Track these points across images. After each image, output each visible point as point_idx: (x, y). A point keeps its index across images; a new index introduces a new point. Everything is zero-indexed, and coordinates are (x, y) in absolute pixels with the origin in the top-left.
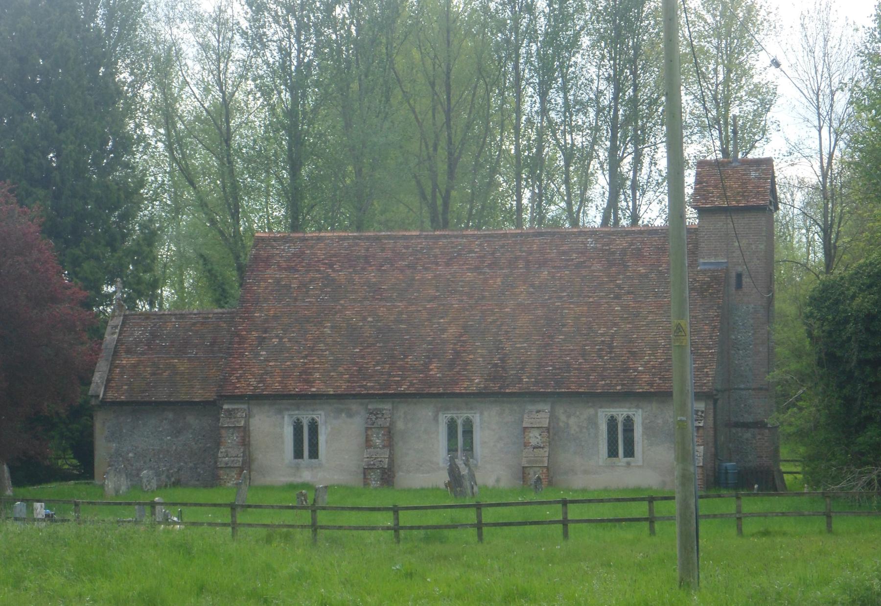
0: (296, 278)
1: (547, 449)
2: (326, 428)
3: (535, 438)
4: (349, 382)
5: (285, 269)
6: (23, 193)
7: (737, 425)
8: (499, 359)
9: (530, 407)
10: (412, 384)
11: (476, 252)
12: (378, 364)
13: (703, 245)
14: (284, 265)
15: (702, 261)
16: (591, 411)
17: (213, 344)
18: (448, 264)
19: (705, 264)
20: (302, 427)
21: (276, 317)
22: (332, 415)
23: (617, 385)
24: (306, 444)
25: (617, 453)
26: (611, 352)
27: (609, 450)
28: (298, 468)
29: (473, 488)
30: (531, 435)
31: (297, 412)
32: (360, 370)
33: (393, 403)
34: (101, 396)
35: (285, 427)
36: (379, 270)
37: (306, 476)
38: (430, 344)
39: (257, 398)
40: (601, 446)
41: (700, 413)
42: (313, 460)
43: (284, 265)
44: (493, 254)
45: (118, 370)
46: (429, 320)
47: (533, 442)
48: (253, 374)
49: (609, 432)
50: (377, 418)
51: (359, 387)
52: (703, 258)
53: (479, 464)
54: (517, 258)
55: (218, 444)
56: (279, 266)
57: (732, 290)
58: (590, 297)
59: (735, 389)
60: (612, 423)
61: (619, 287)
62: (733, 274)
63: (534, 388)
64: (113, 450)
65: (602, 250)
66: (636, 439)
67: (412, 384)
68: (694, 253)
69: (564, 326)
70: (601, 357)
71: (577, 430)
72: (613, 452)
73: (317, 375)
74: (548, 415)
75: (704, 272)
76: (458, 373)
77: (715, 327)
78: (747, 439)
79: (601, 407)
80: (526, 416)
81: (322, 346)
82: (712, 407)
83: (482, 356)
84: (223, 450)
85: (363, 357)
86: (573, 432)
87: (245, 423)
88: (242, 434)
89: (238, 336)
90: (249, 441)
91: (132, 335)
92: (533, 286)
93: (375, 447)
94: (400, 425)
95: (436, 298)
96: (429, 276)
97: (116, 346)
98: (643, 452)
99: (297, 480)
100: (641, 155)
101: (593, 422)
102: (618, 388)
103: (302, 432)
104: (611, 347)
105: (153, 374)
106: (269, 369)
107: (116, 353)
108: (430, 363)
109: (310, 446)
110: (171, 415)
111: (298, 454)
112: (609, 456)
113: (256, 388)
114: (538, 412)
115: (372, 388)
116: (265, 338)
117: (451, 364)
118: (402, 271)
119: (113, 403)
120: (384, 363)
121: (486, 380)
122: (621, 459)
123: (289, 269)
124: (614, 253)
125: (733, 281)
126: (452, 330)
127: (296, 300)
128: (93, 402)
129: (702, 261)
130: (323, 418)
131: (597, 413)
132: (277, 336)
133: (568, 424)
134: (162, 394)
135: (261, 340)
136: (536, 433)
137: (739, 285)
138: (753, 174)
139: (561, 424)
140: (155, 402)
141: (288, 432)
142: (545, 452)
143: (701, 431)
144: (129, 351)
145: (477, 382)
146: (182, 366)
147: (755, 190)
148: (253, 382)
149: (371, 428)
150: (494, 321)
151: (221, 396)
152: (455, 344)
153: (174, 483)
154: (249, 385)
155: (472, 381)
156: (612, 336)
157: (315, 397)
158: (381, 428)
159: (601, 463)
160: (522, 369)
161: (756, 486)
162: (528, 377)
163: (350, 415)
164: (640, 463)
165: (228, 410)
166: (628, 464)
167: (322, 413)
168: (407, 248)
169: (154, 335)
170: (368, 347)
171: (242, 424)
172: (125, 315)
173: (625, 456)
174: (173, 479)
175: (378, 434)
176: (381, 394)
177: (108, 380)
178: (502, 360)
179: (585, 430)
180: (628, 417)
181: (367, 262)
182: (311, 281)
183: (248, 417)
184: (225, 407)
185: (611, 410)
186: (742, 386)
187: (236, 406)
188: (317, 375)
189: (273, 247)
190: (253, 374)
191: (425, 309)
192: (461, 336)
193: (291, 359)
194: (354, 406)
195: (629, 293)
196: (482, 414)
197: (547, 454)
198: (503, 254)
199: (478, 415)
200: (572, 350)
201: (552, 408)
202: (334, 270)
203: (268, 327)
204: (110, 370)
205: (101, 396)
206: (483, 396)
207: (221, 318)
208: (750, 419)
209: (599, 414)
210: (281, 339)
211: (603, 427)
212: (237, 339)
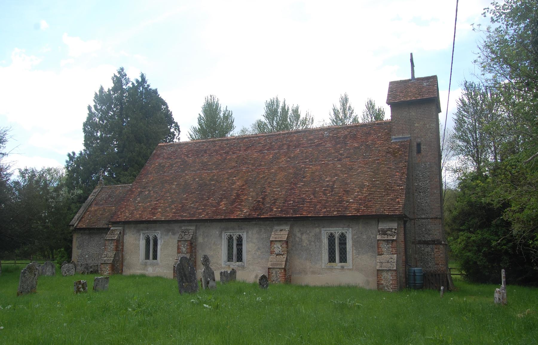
1: (285, 256)
2: (161, 242)
3: (278, 248)
7: (420, 242)
8: (262, 198)
9: (276, 228)
10: (207, 214)
13: (394, 127)
14: (166, 157)
15: (394, 137)
16: (317, 230)
18: (245, 150)
19: (396, 139)
23: (334, 211)
24: (152, 251)
25: (335, 260)
26: (332, 191)
27: (330, 258)
28: (146, 265)
29: (208, 283)
30: (275, 246)
33: (196, 226)
34: (75, 225)
35: (141, 240)
36: (210, 155)
37: (150, 271)
38: (224, 191)
39: (126, 223)
41: (393, 230)
42: (154, 261)
43: (166, 157)
46: (228, 178)
47: (277, 251)
49: (329, 245)
52: (395, 135)
57: (415, 153)
58: (322, 161)
59: (418, 218)
60: (331, 238)
61: (341, 154)
62: (415, 144)
63: (279, 215)
65: (333, 137)
66: (348, 249)
68: (389, 134)
69: (304, 177)
70: (325, 194)
71: (308, 243)
72: (332, 259)
74: (287, 233)
75: (395, 143)
76: (235, 207)
77: (404, 173)
78: (428, 252)
80: (273, 233)
81: (168, 194)
82: (403, 226)
83: (252, 197)
85: (187, 200)
86: (305, 244)
93: (183, 253)
94: (200, 240)
98: (353, 260)
100: (425, 241)
101: (318, 238)
102: (335, 213)
104: (332, 188)
105: (102, 214)
108: (221, 201)
111: (147, 257)
112: (330, 262)
114: (281, 230)
115: (185, 216)
117: (234, 202)
118: (221, 155)
119: (80, 229)
121: (251, 210)
122: (338, 264)
124: (339, 138)
125: (415, 148)
129: (394, 137)
131: (321, 231)
133: (301, 239)
136: (278, 245)
137: (419, 151)
138: (425, 84)
139: (297, 239)
140: (96, 228)
141: (142, 243)
142: (283, 258)
143: (394, 243)
145: (246, 211)
147: (427, 91)
149: (181, 241)
150: (264, 177)
152: (238, 190)
153: (91, 272)
155: (242, 211)
156: (334, 182)
157: (155, 222)
158: (186, 241)
160: (274, 203)
161: (442, 288)
164: (351, 267)
166: (343, 267)
168: (227, 144)
175: (184, 245)
178: (264, 199)
179: (313, 243)
180: (342, 234)
181: (205, 152)
185: (331, 229)
186: (423, 216)
189: (164, 149)
191: (227, 173)
192: (243, 186)
195: (347, 157)
197: (285, 259)
198: (276, 143)
199: (245, 233)
200: (307, 191)
201: (291, 228)
205: (75, 225)
206: (247, 220)
208: (429, 238)
209: (322, 232)
211: (325, 241)
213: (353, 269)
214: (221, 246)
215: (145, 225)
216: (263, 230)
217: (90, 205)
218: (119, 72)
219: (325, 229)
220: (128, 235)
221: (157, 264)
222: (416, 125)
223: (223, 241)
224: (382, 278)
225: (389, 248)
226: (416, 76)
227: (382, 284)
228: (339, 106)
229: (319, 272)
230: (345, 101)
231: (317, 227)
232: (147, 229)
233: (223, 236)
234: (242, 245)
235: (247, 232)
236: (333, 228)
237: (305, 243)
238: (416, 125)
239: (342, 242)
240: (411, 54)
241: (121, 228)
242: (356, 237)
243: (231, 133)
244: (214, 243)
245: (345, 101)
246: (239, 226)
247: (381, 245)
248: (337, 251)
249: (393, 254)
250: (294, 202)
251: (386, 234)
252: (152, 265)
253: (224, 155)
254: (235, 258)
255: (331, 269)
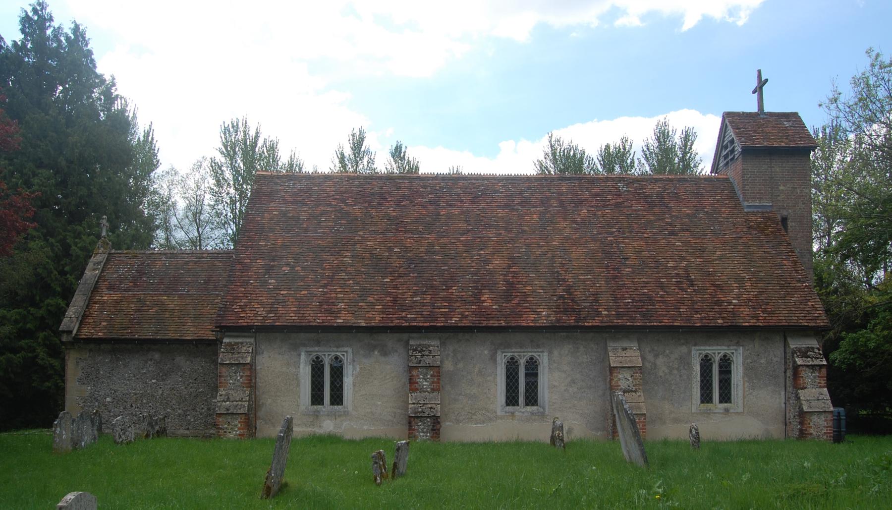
0: (305, 211)
2: (354, 369)
4: (383, 313)
5: (292, 203)
6: (30, 173)
10: (464, 317)
11: (502, 192)
12: (415, 294)
16: (684, 349)
17: (207, 282)
20: (323, 366)
21: (284, 246)
22: (362, 352)
25: (322, 399)
27: (313, 396)
28: (316, 415)
30: (621, 376)
31: (317, 349)
32: (395, 300)
34: (75, 332)
35: (302, 366)
37: (328, 426)
38: (476, 274)
40: (694, 390)
44: (520, 194)
45: (97, 306)
48: (261, 303)
50: (423, 356)
51: (398, 318)
53: (547, 413)
54: (548, 199)
55: (215, 389)
56: (283, 200)
60: (706, 364)
64: (87, 394)
67: (464, 317)
71: (667, 371)
72: (706, 398)
73: (342, 305)
76: (518, 305)
79: (695, 345)
83: (542, 287)
84: (222, 392)
85: (396, 287)
86: (661, 373)
87: (252, 359)
88: (248, 373)
89: (241, 263)
90: (255, 383)
91: (117, 272)
92: (575, 222)
93: (422, 391)
95: (469, 231)
96: (457, 212)
97: (97, 282)
98: (744, 397)
99: (319, 431)
101: (685, 361)
103: (323, 373)
106: (281, 297)
107: (96, 289)
108: (481, 293)
109: (332, 390)
110: (157, 356)
111: (317, 398)
113: (265, 318)
114: (624, 349)
115: (414, 320)
116: (273, 266)
117: (508, 296)
119: (89, 341)
120: (424, 293)
122: (717, 406)
123: (295, 202)
126: (497, 262)
127: (306, 230)
128: (64, 338)
130: (350, 356)
131: (690, 351)
132: (288, 265)
133: (655, 364)
134: (147, 332)
135: (269, 269)
140: (138, 340)
144: (111, 288)
145: (545, 316)
146: (172, 303)
148: (261, 311)
151: (221, 327)
154: (256, 315)
159: (694, 411)
162: (606, 310)
163: (385, 353)
164: (740, 410)
165: (229, 344)
166: (727, 410)
167: (350, 350)
169: (141, 273)
170: (400, 277)
171: (248, 360)
172: (109, 254)
173: (332, 403)
174: (157, 428)
175: (425, 375)
176: (427, 327)
177: (85, 316)
179: (676, 372)
182: (322, 214)
183: (255, 353)
184: (226, 340)
185: (708, 348)
187: (240, 340)
188: (342, 305)
190: (261, 303)
192: (510, 267)
193: (307, 287)
194: (390, 341)
196: (550, 353)
199: (546, 354)
200: (647, 283)
202: (347, 205)
203: (276, 256)
204: (87, 306)
205: (75, 332)
207: (217, 257)
209: (693, 352)
210: (293, 267)
211: (697, 368)
212: (238, 267)
213: (743, 413)
214: (495, 378)
215: (312, 335)
216: (582, 349)
217: (96, 289)
218: (35, 11)
219: (697, 348)
220: (266, 354)
221: (346, 413)
222: (781, 188)
223: (499, 369)
224: (811, 424)
225: (815, 377)
226: (767, 109)
227: (811, 434)
228: (348, 152)
229: (683, 416)
230: (358, 144)
231: (683, 344)
232: (318, 343)
233: (499, 358)
234: (536, 375)
235: (550, 353)
236: (713, 345)
237: (662, 371)
238: (781, 188)
239: (724, 369)
240: (759, 72)
241: (252, 340)
242: (749, 361)
243: (595, 160)
244: (480, 371)
245: (358, 144)
246: (532, 341)
247: (803, 374)
248: (716, 384)
249: (820, 387)
250: (634, 301)
251: (808, 357)
252: (333, 416)
253: (431, 208)
254: (521, 399)
255: (708, 413)
